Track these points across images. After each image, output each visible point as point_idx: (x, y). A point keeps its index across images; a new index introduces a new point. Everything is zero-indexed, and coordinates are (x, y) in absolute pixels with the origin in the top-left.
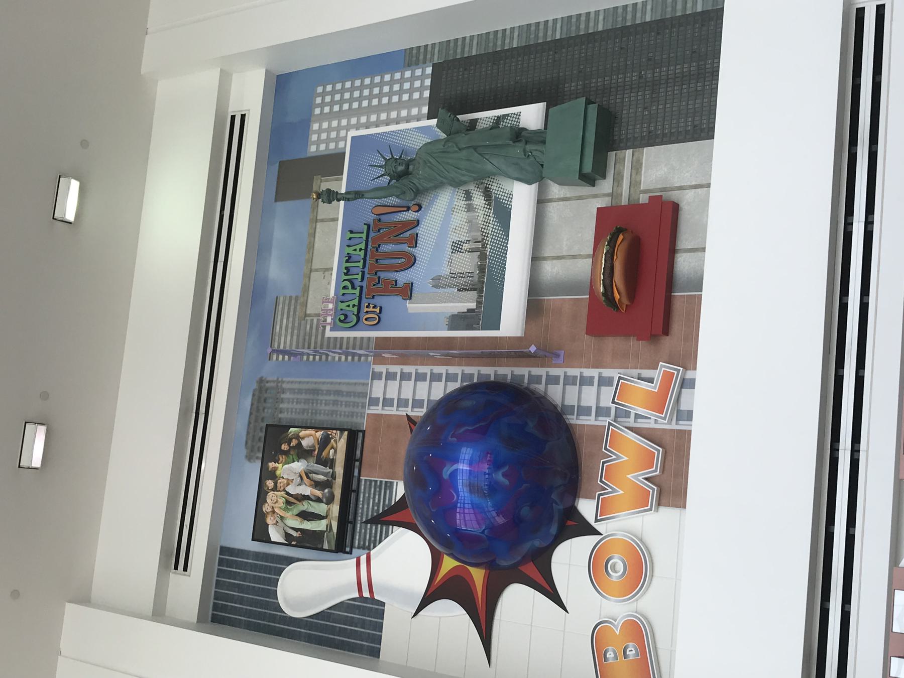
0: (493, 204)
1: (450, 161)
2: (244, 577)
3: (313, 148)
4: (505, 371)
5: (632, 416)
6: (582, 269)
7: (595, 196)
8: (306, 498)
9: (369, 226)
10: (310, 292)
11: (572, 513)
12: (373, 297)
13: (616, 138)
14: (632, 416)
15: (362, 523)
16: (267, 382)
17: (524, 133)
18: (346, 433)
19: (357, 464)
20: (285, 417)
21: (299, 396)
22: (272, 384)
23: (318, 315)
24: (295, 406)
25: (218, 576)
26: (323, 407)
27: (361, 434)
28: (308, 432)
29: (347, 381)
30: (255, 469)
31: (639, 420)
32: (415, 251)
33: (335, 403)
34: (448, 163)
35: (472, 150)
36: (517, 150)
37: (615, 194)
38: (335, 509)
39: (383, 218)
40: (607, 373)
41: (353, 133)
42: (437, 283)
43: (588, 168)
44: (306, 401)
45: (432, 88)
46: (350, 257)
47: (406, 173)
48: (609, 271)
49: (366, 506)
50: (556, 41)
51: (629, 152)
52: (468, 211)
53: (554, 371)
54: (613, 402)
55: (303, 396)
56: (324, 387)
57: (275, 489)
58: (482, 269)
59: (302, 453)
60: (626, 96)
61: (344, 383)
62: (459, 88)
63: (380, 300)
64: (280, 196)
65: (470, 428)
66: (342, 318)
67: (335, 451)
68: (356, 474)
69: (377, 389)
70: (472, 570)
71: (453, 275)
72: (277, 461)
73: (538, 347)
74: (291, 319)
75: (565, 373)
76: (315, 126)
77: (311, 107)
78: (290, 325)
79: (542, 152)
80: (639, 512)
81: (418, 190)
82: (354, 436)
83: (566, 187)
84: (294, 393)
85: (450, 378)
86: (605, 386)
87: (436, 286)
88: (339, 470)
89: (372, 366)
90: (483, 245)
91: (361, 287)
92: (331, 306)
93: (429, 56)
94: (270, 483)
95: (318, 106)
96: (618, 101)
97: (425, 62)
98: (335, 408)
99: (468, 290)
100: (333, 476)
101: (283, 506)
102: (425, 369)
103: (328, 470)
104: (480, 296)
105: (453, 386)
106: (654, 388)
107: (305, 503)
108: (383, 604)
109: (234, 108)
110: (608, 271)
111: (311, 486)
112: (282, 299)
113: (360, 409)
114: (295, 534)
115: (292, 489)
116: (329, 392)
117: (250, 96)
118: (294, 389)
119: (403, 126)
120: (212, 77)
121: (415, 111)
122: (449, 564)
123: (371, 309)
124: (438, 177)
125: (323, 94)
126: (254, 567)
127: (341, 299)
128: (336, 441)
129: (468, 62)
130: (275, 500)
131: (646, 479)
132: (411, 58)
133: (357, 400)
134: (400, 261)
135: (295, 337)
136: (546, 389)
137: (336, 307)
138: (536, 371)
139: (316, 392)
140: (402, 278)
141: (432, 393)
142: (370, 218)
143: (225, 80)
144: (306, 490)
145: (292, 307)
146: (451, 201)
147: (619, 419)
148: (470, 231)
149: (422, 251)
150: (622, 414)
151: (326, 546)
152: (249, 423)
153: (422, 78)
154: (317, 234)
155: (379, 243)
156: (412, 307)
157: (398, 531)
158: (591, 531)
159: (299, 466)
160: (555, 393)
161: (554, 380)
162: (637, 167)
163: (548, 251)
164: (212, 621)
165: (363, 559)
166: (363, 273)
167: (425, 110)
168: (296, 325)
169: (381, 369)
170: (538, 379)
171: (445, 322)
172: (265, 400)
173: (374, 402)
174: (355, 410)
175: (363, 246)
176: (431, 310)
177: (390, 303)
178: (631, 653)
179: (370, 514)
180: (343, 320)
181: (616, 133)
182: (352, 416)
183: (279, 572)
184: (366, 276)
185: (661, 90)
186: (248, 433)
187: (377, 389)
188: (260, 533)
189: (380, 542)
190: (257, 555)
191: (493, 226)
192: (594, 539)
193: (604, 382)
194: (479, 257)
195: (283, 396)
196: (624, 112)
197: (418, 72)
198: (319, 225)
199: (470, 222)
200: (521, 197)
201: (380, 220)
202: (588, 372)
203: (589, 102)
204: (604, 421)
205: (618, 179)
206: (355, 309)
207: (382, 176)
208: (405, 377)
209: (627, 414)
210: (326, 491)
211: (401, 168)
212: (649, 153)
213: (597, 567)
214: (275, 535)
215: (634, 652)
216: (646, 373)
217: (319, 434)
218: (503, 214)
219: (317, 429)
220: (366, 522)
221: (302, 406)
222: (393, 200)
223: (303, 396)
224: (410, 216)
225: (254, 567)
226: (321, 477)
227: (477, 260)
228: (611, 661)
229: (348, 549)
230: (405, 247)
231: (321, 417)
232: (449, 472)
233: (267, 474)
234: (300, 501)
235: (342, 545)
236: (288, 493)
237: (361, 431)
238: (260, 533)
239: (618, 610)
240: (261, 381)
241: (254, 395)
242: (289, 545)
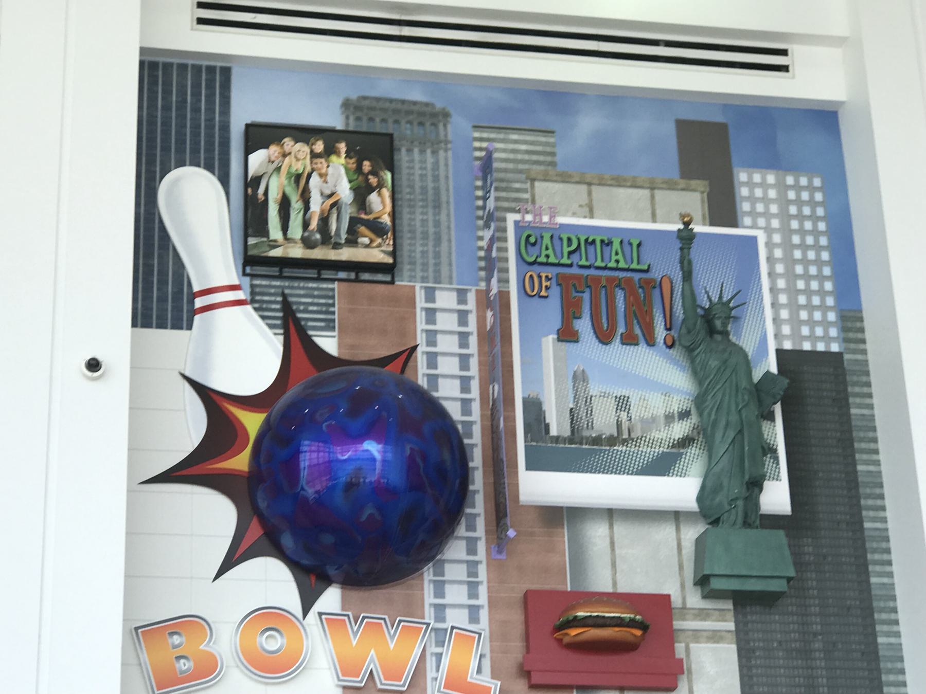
0: (674, 450)
4: (478, 482)
5: (439, 650)
6: (601, 580)
7: (683, 586)
8: (307, 208)
9: (647, 271)
11: (327, 581)
12: (558, 285)
14: (439, 650)
15: (283, 287)
18: (391, 261)
20: (402, 157)
21: (430, 178)
22: (442, 133)
23: (533, 201)
24: (418, 172)
25: (193, 66)
26: (419, 217)
27: (388, 278)
28: (388, 201)
29: (454, 249)
30: (334, 119)
31: (434, 659)
33: (425, 235)
36: (737, 489)
37: (686, 611)
38: (297, 252)
40: (484, 614)
42: (580, 378)
43: (716, 584)
44: (424, 189)
45: (813, 353)
46: (608, 245)
47: (711, 331)
49: (302, 292)
50: (861, 522)
53: (481, 547)
54: (453, 628)
56: (443, 217)
57: (314, 156)
58: (597, 441)
59: (361, 193)
62: (812, 393)
63: (555, 292)
64: (685, 128)
65: (421, 470)
66: (532, 240)
67: (367, 246)
70: (247, 453)
71: (589, 400)
76: (771, 179)
78: (519, 157)
79: (734, 524)
80: (333, 661)
81: (693, 350)
82: (388, 270)
83: (693, 548)
84: (433, 170)
85: (466, 404)
87: (575, 377)
88: (346, 254)
89: (474, 289)
91: (571, 266)
92: (546, 219)
93: (852, 346)
95: (797, 181)
96: (790, 608)
98: (418, 235)
99: (572, 423)
100: (337, 246)
101: (293, 170)
102: (474, 370)
103: (344, 236)
104: (564, 440)
108: (190, 327)
109: (798, 55)
110: (600, 621)
111: (322, 212)
112: (552, 140)
113: (419, 274)
114: (261, 191)
115: (315, 181)
116: (437, 224)
118: (438, 169)
119: (768, 313)
120: (839, 28)
121: (786, 330)
122: (252, 422)
123: (544, 284)
125: (811, 188)
126: (210, 121)
127: (557, 235)
128: (379, 246)
129: (842, 402)
130: (299, 154)
131: (371, 671)
132: (851, 321)
134: (604, 320)
138: (481, 523)
139: (437, 206)
140: (584, 326)
142: (656, 274)
144: (316, 205)
145: (541, 158)
146: (678, 391)
147: (433, 634)
148: (642, 420)
149: (618, 355)
150: (441, 637)
151: (252, 241)
152: (391, 101)
156: (549, 341)
157: (278, 343)
158: (306, 608)
159: (345, 192)
160: (455, 550)
161: (472, 550)
162: (715, 637)
163: (621, 529)
166: (589, 267)
167: (788, 345)
168: (521, 166)
169: (471, 304)
170: (471, 527)
172: (421, 124)
175: (622, 265)
178: (184, 665)
179: (310, 324)
180: (529, 240)
182: (410, 263)
183: (209, 168)
184: (586, 272)
185: (800, 662)
186: (378, 99)
187: (446, 299)
189: (263, 318)
190: (225, 128)
191: (648, 452)
192: (298, 611)
193: (474, 612)
194: (611, 436)
195: (429, 151)
196: (777, 617)
197: (833, 332)
198: (646, 193)
199: (654, 419)
201: (654, 288)
202: (483, 590)
203: (789, 579)
204: (429, 615)
205: (702, 614)
206: (542, 259)
207: (709, 297)
209: (440, 643)
210: (318, 236)
211: (718, 324)
212: (730, 651)
213: (267, 618)
214: (258, 159)
215: (184, 668)
217: (386, 219)
218: (662, 465)
219: (394, 215)
220: (284, 296)
221: (418, 184)
222: (679, 312)
223: (431, 185)
224: (660, 333)
226: (333, 227)
227: (608, 434)
228: (170, 641)
229: (248, 270)
230: (621, 329)
231: (406, 210)
233: (330, 136)
235: (251, 262)
236: (309, 176)
237: (393, 278)
238: (260, 135)
239: (225, 643)
240: (446, 115)
241: (427, 105)
242: (247, 185)
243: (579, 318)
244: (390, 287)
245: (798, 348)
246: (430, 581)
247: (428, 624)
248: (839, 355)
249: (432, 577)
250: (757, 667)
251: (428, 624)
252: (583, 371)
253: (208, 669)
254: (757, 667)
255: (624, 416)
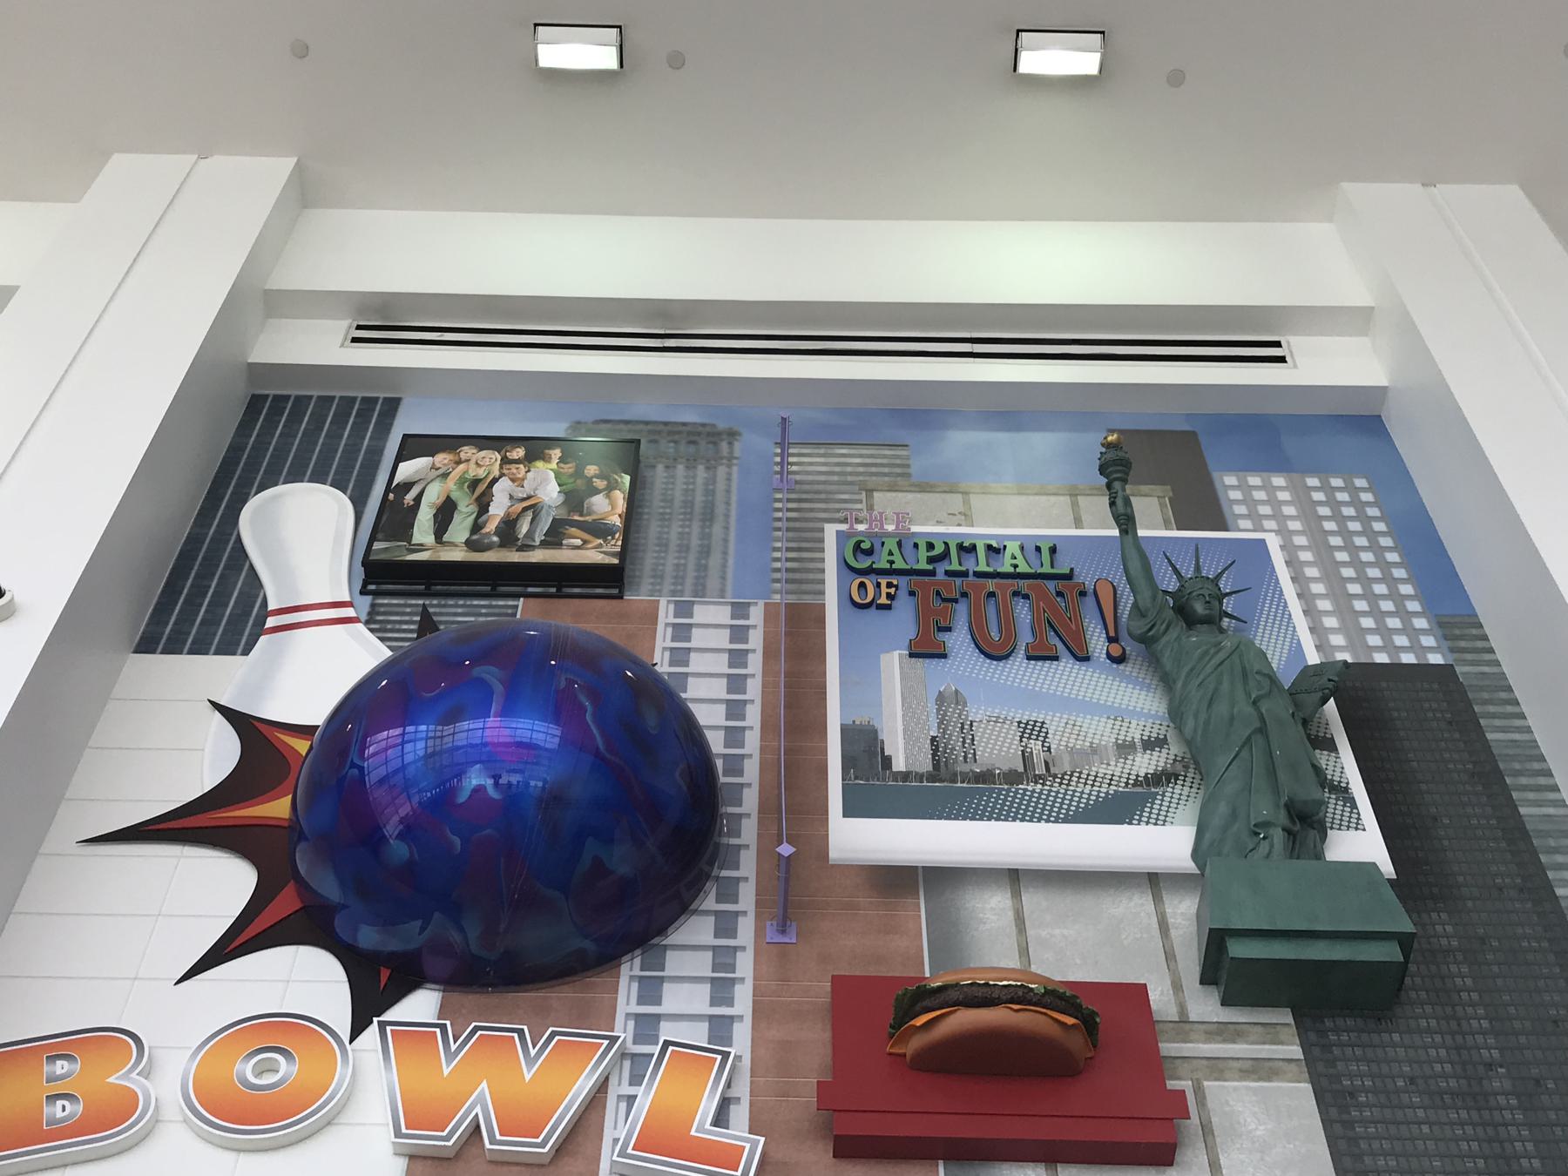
0: (1139, 790)
1: (1225, 686)
2: (334, 436)
3: (1230, 480)
7: (1177, 987)
10: (919, 495)
11: (406, 981)
12: (912, 594)
13: (1328, 1023)
14: (631, 1091)
16: (730, 443)
17: (1312, 833)
18: (616, 561)
19: (553, 590)
27: (615, 591)
31: (623, 1105)
32: (1018, 662)
33: (684, 549)
34: (1219, 682)
35: (1257, 725)
38: (458, 555)
39: (1090, 601)
41: (1273, 543)
42: (949, 701)
43: (1238, 949)
44: (688, 504)
45: (1396, 669)
48: (983, 996)
51: (1296, 1051)
52: (1118, 746)
53: (746, 930)
54: (667, 1044)
55: (699, 498)
57: (505, 461)
58: (986, 777)
60: (1438, 1038)
61: (725, 560)
67: (578, 548)
68: (530, 590)
69: (712, 614)
71: (967, 728)
72: (562, 460)
73: (800, 886)
74: (861, 469)
75: (743, 948)
76: (1278, 481)
77: (1323, 471)
78: (849, 469)
79: (1268, 856)
81: (1155, 640)
86: (710, 1030)
87: (941, 699)
88: (538, 556)
90: (1040, 777)
92: (890, 528)
94: (519, 453)
97: (1452, 650)
99: (934, 755)
100: (525, 548)
104: (920, 777)
105: (716, 743)
106: (701, 1125)
107: (474, 508)
109: (1294, 344)
110: (980, 993)
111: (508, 514)
114: (409, 498)
116: (706, 536)
117: (1321, 364)
119: (1295, 607)
120: (1354, 292)
124: (1186, 669)
126: (352, 450)
129: (1467, 725)
132: (1459, 626)
133: (689, 582)
135: (823, 478)
136: (707, 913)
137: (889, 535)
138: (747, 898)
139: (708, 516)
141: (704, 706)
142: (1086, 578)
143: (1353, 320)
144: (499, 508)
145: (886, 470)
146: (1140, 715)
147: (627, 1064)
148: (1072, 751)
149: (1018, 670)
150: (638, 1067)
153: (1415, 647)
154: (1044, 498)
155: (1033, 595)
156: (893, 663)
160: (696, 930)
161: (726, 925)
162: (1259, 1070)
163: (1033, 900)
164: (253, 396)
165: (349, 612)
169: (756, 615)
170: (729, 892)
171: (861, 718)
173: (684, 609)
174: (668, 580)
176: (883, 691)
177: (903, 620)
180: (862, 559)
181: (1340, 1022)
183: (339, 485)
188: (413, 446)
191: (1084, 792)
192: (343, 1026)
199: (1094, 750)
200: (1166, 842)
203: (1405, 941)
204: (624, 1031)
205: (1222, 1032)
208: (738, 658)
209: (636, 1080)
210: (495, 539)
211: (1199, 608)
212: (1299, 1096)
213: (277, 1031)
214: (407, 470)
215: (60, 1114)
216: (740, 1115)
217: (616, 521)
218: (1119, 808)
219: (630, 516)
224: (1098, 643)
225: (352, 450)
227: (1005, 768)
228: (46, 1068)
229: (372, 587)
232: (484, 676)
234: (477, 500)
236: (495, 481)
239: (166, 1083)
240: (732, 435)
241: (703, 425)
242: (388, 490)
243: (949, 629)
244: (614, 602)
245: (1363, 660)
246: (632, 978)
247: (614, 1040)
248: (1446, 671)
249: (637, 972)
250: (1365, 1122)
251: (614, 1040)
252: (957, 691)
253: (112, 1117)
254: (1365, 1122)
255: (1035, 746)
